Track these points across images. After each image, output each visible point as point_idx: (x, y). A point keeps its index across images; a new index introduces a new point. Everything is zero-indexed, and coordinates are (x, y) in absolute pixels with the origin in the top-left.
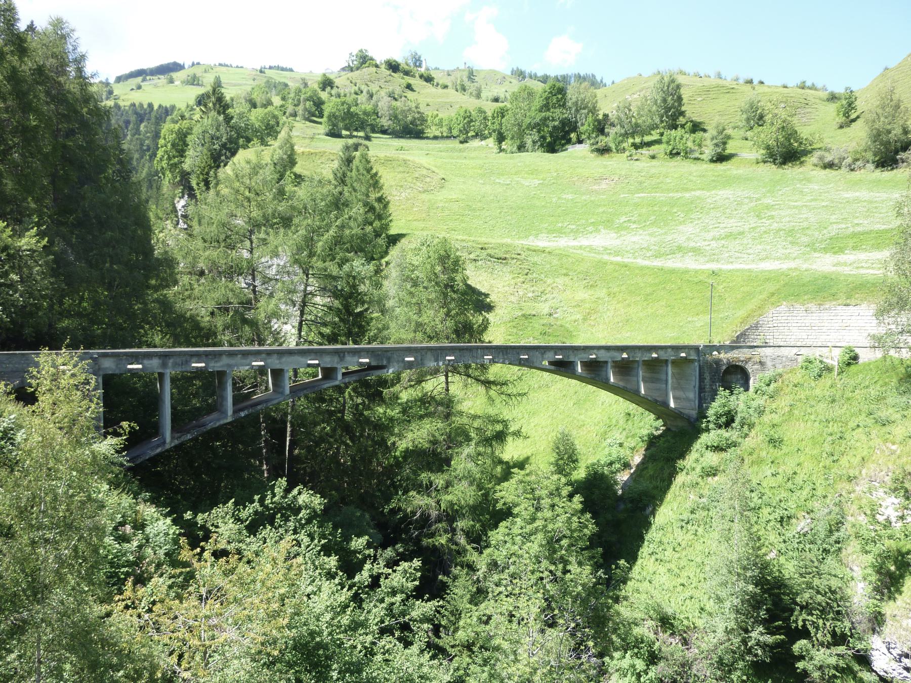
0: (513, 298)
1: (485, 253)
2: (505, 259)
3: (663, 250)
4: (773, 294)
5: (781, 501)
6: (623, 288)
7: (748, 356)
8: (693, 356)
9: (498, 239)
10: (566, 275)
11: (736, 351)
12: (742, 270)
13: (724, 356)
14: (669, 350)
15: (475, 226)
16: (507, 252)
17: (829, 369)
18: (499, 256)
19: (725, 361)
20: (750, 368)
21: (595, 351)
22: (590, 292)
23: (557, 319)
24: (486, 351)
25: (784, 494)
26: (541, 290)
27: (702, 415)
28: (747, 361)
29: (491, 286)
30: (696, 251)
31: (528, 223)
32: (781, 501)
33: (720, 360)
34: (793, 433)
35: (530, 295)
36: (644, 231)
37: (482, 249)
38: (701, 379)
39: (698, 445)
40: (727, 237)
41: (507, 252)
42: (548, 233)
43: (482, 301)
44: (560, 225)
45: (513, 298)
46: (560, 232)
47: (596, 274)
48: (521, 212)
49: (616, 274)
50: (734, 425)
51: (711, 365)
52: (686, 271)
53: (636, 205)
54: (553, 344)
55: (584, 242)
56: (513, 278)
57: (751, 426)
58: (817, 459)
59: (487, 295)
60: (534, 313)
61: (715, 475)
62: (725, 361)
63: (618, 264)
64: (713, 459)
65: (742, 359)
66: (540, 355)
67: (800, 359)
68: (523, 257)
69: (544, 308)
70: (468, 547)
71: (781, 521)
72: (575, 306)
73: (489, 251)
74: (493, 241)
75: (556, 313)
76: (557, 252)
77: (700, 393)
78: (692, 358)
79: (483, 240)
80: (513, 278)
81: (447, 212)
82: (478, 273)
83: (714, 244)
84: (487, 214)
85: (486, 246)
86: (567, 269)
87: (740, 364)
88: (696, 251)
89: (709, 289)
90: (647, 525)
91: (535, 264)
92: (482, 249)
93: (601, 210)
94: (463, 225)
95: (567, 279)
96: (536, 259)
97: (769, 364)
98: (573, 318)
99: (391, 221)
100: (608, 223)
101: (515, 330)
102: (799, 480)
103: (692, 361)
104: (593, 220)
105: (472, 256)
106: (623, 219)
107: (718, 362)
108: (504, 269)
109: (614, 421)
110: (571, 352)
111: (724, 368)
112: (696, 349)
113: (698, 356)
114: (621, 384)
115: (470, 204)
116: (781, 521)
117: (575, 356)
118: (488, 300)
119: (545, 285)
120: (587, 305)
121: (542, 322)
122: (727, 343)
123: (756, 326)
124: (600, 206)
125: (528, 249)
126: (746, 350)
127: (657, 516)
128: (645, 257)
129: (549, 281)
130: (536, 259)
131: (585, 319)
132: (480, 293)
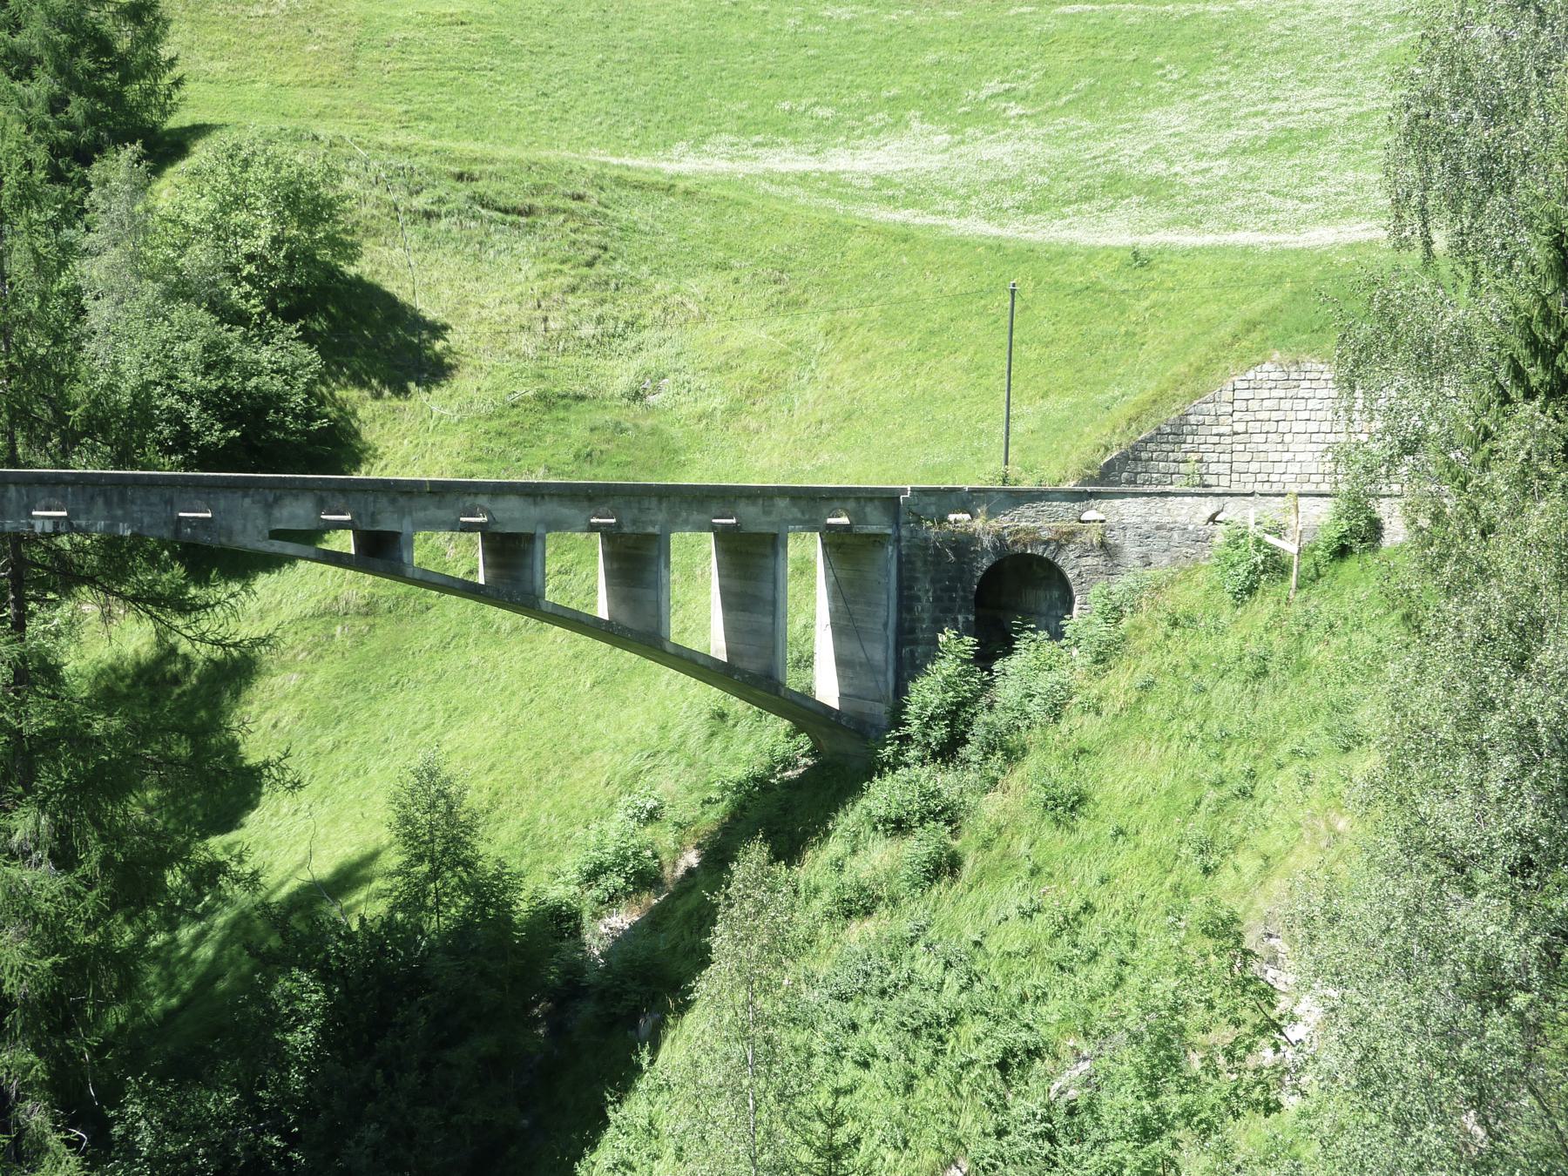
0: (524, 343)
1: (466, 189)
2: (529, 211)
3: (1061, 188)
4: (1251, 326)
5: (1023, 999)
6: (874, 312)
7: (1065, 527)
8: (877, 523)
9: (516, 143)
10: (721, 266)
11: (1027, 510)
12: (1223, 250)
13: (981, 525)
14: (782, 503)
15: (505, 104)
16: (538, 190)
17: (1276, 566)
18: (510, 203)
19: (987, 542)
20: (1070, 564)
21: (483, 500)
22: (779, 323)
23: (650, 409)
24: (40, 492)
25: (1039, 977)
26: (627, 315)
27: (897, 717)
28: (1063, 540)
29: (464, 301)
30: (1155, 190)
31: (685, 97)
32: (1023, 999)
33: (972, 539)
34: (1119, 781)
35: (588, 330)
36: (1041, 125)
37: (460, 177)
38: (906, 601)
39: (848, 820)
40: (1272, 143)
41: (538, 190)
42: (741, 132)
43: (418, 349)
44: (786, 106)
45: (524, 343)
46: (782, 129)
47: (802, 266)
48: (670, 62)
49: (869, 266)
50: (964, 752)
51: (939, 553)
52: (1062, 255)
53: (1046, 39)
54: (516, 480)
55: (839, 161)
56: (541, 276)
57: (1013, 755)
58: (1165, 862)
59: (438, 330)
60: (579, 389)
61: (868, 912)
62: (987, 542)
63: (883, 232)
64: (881, 858)
65: (1045, 535)
66: (257, 510)
67: (1220, 534)
68: (592, 205)
69: (620, 374)
70: (53, 1140)
71: (1003, 1066)
72: (719, 370)
73: (481, 187)
74: (503, 152)
75: (657, 390)
76: (715, 191)
77: (899, 645)
78: (873, 529)
79: (467, 147)
80: (541, 276)
81: (417, 59)
82: (431, 257)
83: (1221, 167)
84: (555, 68)
85: (476, 169)
86: (728, 246)
87: (1039, 551)
88: (1155, 190)
89: (1010, 293)
90: (624, 1077)
91: (628, 230)
92: (460, 177)
93: (931, 57)
94: (463, 102)
95: (720, 279)
96: (637, 213)
97: (1131, 551)
98: (703, 405)
99: (178, 83)
100: (940, 103)
101: (499, 445)
102: (1091, 932)
103: (877, 540)
104: (894, 91)
105: (420, 202)
106: (993, 85)
107: (964, 545)
108: (520, 247)
109: (674, 735)
110: (383, 501)
111: (985, 563)
112: (888, 500)
113: (896, 523)
114: (624, 618)
115: (506, 32)
116: (1003, 1066)
117: (402, 513)
118: (439, 345)
119: (645, 299)
120: (753, 367)
121: (601, 418)
122: (1070, 485)
123: (1177, 432)
124: (927, 43)
125: (620, 182)
126: (1059, 507)
127: (666, 1046)
128: (995, 212)
129: (661, 287)
130: (637, 213)
131: (733, 412)
132: (417, 323)
